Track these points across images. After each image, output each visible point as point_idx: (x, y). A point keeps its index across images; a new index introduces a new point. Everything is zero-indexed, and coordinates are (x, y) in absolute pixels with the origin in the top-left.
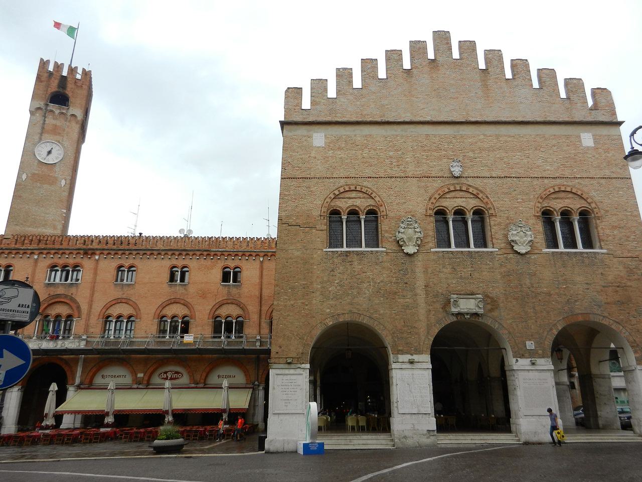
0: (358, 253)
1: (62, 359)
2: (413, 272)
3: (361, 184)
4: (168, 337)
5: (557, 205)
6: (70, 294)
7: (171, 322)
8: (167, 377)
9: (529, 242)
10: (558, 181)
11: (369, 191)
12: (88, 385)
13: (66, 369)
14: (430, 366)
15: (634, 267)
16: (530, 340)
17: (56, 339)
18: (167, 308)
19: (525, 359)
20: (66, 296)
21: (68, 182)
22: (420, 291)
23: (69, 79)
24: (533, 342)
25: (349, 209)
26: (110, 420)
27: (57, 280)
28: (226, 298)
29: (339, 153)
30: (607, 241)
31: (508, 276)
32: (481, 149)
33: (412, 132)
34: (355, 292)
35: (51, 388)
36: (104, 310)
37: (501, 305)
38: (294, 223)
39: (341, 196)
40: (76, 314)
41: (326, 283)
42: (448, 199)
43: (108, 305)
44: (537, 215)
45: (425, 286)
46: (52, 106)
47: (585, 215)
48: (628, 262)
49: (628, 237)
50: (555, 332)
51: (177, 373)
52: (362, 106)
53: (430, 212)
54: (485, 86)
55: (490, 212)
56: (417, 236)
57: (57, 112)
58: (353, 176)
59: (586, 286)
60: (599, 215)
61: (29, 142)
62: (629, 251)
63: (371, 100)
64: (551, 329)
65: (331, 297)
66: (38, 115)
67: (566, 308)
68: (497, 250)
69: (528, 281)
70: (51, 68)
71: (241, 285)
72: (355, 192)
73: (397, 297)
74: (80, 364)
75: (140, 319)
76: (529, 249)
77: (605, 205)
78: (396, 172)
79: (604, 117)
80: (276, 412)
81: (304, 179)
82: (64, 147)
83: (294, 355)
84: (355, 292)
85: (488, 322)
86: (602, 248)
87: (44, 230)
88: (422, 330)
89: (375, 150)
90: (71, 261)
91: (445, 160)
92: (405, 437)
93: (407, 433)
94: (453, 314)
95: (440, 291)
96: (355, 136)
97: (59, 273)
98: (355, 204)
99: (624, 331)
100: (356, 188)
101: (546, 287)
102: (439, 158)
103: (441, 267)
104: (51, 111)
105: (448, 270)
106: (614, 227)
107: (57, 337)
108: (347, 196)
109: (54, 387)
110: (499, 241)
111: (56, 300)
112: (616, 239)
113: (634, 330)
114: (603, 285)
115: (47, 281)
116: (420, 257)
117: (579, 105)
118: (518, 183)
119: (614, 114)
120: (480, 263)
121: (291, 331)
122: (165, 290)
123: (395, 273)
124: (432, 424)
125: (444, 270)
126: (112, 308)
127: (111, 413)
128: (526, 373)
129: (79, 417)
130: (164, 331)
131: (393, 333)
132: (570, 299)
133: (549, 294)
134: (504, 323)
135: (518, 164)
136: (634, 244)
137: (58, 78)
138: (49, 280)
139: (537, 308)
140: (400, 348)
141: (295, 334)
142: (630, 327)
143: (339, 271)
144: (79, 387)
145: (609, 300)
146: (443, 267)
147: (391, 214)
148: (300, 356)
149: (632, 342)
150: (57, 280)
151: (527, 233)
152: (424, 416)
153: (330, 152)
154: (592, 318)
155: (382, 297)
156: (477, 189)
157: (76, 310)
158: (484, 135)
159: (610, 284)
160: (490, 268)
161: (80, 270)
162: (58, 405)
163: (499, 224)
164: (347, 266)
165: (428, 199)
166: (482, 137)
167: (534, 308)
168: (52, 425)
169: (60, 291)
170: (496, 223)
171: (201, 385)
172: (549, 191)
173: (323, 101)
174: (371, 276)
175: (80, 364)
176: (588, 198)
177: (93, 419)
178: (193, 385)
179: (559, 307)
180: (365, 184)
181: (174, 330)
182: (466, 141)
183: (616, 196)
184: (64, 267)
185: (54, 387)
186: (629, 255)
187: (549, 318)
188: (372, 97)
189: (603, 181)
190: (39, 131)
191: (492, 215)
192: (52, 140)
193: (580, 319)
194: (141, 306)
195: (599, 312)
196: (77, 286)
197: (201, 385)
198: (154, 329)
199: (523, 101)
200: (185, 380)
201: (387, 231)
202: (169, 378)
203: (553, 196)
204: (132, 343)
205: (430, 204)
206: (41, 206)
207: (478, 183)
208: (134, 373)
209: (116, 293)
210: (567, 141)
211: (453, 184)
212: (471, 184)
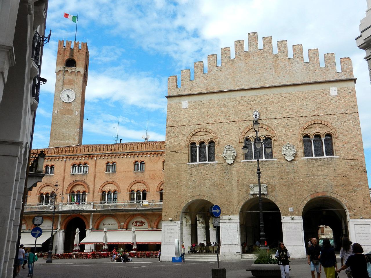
0: (204, 165)
1: (82, 215)
2: (231, 173)
3: (206, 127)
4: (135, 202)
5: (312, 132)
6: (83, 180)
7: (137, 194)
8: (137, 224)
9: (293, 154)
10: (314, 118)
11: (210, 131)
12: (97, 228)
13: (85, 220)
14: (239, 221)
15: (354, 165)
16: (291, 207)
17: (78, 205)
18: (134, 185)
19: (288, 217)
20: (81, 181)
21: (79, 112)
22: (235, 183)
23: (75, 50)
24: (293, 208)
25: (200, 141)
26: (105, 247)
27: (76, 172)
29: (195, 111)
32: (271, 103)
33: (234, 96)
34: (202, 184)
35: (76, 231)
36: (101, 188)
37: (277, 189)
38: (173, 150)
40: (87, 191)
41: (188, 180)
42: (251, 133)
43: (103, 185)
44: (300, 138)
45: (237, 180)
46: (68, 69)
47: (329, 136)
48: (352, 162)
49: (353, 148)
50: (306, 202)
51: (142, 222)
53: (241, 140)
54: (276, 63)
56: (233, 155)
57: (70, 71)
58: (202, 123)
59: (324, 177)
60: (336, 136)
61: (57, 91)
62: (352, 156)
63: (213, 79)
64: (303, 201)
65: (190, 188)
66: (61, 74)
67: (312, 189)
68: (276, 159)
70: (65, 45)
72: (203, 132)
73: (223, 186)
74: (91, 217)
75: (120, 192)
76: (293, 158)
77: (340, 130)
78: (224, 119)
79: (345, 76)
80: (165, 243)
81: (178, 127)
82: (75, 92)
83: (173, 217)
84: (202, 184)
85: (269, 197)
86: (336, 155)
87: (69, 142)
88: (235, 203)
90: (83, 161)
91: (251, 111)
92: (225, 255)
93: (226, 254)
94: (251, 194)
96: (203, 101)
97: (77, 168)
98: (203, 138)
99: (344, 201)
100: (203, 130)
101: (302, 179)
102: (247, 110)
103: (246, 170)
104: (67, 71)
105: (250, 171)
106: (345, 143)
107: (79, 203)
109: (77, 231)
110: (278, 154)
111: (77, 183)
112: (345, 149)
113: (350, 200)
114: (335, 176)
115: (71, 173)
116: (235, 165)
117: (330, 70)
118: (291, 120)
119: (352, 73)
120: (266, 167)
121: (172, 205)
122: (132, 176)
123: (222, 174)
124: (239, 249)
125: (248, 171)
126: (105, 187)
127: (106, 244)
128: (288, 224)
129: (93, 246)
130: (133, 199)
132: (315, 184)
133: (304, 182)
134: (278, 198)
137: (70, 50)
138: (73, 173)
139: (296, 190)
140: (224, 212)
141: (173, 206)
144: (92, 230)
145: (337, 184)
146: (247, 170)
147: (221, 143)
148: (176, 217)
149: (349, 207)
150: (76, 172)
151: (292, 149)
152: (235, 245)
153: (191, 111)
155: (215, 187)
156: (267, 126)
157: (87, 188)
158: (274, 94)
159: (339, 175)
161: (87, 166)
162: (81, 240)
163: (279, 145)
164: (198, 172)
165: (240, 133)
166: (272, 95)
167: (295, 190)
168: (78, 250)
169: (78, 178)
171: (155, 229)
173: (187, 82)
174: (210, 176)
175: (91, 217)
176: (331, 126)
177: (98, 246)
178: (150, 229)
179: (309, 189)
180: (208, 127)
181: (138, 198)
182: (263, 98)
183: (348, 124)
184: (79, 165)
185: (77, 231)
186: (352, 158)
187: (303, 195)
188: (213, 77)
189: (341, 116)
190: (62, 84)
191: (275, 140)
192: (69, 88)
193: (320, 195)
194: (120, 185)
195: (331, 191)
196: (87, 175)
197: (124, 230)
198: (127, 198)
199: (297, 71)
200: (146, 226)
201: (218, 152)
202: (138, 225)
203: (311, 127)
204: (116, 206)
206: (66, 128)
207: (268, 122)
208: (119, 222)
209: (106, 178)
210: (322, 93)
212: (264, 123)
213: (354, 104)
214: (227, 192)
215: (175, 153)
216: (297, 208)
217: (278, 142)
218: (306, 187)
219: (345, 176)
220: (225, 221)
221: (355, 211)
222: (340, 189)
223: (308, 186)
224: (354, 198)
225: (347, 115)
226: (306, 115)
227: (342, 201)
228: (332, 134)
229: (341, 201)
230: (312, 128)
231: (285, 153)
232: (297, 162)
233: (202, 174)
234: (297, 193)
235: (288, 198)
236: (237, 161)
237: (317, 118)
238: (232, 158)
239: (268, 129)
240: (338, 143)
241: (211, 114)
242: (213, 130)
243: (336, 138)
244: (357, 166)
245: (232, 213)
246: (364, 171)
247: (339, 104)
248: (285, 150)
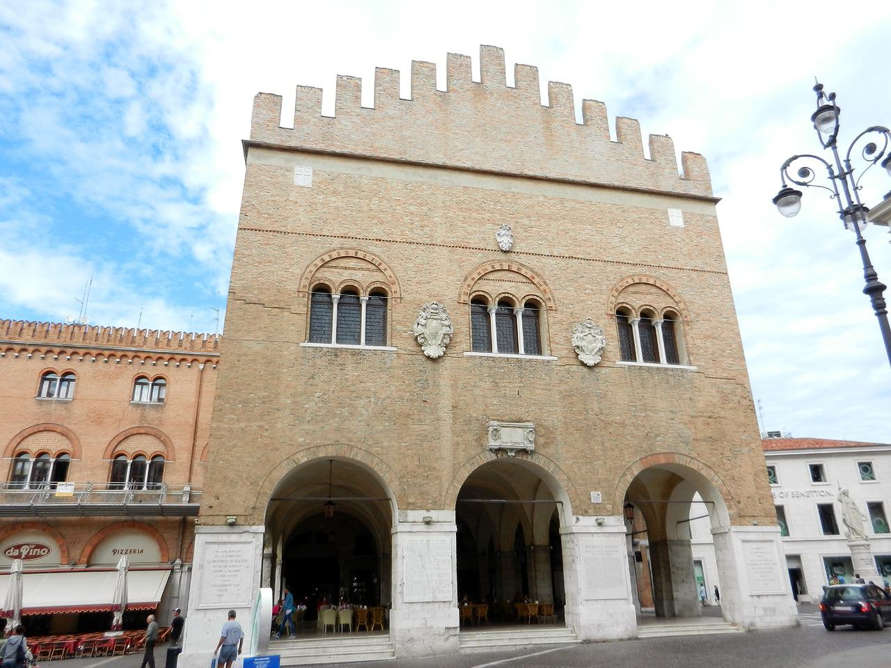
10: (638, 270)
22: (445, 414)
24: (600, 493)
28: (138, 425)
30: (697, 355)
38: (254, 300)
39: (333, 264)
44: (610, 313)
45: (453, 407)
49: (724, 351)
55: (549, 304)
59: (670, 415)
62: (724, 370)
64: (624, 475)
69: (595, 406)
71: (164, 406)
73: (410, 422)
76: (598, 359)
89: (389, 201)
95: (474, 415)
105: (487, 384)
108: (342, 265)
116: (447, 363)
118: (587, 267)
125: (481, 383)
133: (623, 425)
134: (561, 464)
140: (411, 500)
141: (245, 476)
142: (724, 473)
143: (322, 378)
146: (481, 380)
153: (320, 197)
159: (701, 414)
167: (602, 444)
172: (627, 282)
173: (314, 120)
180: (371, 249)
186: (725, 375)
189: (694, 274)
191: (550, 309)
193: (663, 460)
201: (399, 323)
215: (260, 307)
217: (559, 316)
218: (628, 437)
220: (416, 528)
221: (741, 506)
222: (705, 447)
223: (633, 436)
231: (580, 344)
232: (607, 370)
235: (587, 464)
237: (645, 270)
238: (442, 341)
240: (692, 337)
244: (736, 395)
245: (434, 503)
248: (582, 335)
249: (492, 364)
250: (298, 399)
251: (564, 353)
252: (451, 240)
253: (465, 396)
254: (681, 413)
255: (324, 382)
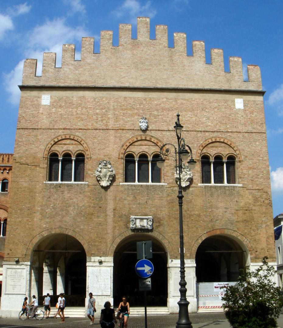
2: (106, 199)
10: (215, 134)
22: (110, 213)
30: (243, 178)
31: (172, 202)
39: (59, 143)
42: (136, 147)
45: (114, 209)
49: (258, 175)
50: (200, 241)
52: (80, 74)
53: (122, 156)
59: (225, 210)
62: (257, 185)
67: (209, 225)
68: (167, 184)
73: (93, 217)
76: (188, 183)
89: (86, 108)
103: (126, 196)
105: (131, 198)
108: (64, 143)
116: (112, 188)
118: (187, 135)
123: (93, 200)
125: (128, 198)
131: (89, 242)
133: (199, 216)
135: (189, 120)
136: (261, 180)
139: (189, 225)
140: (93, 252)
142: (250, 237)
143: (54, 198)
153: (54, 110)
154: (228, 232)
159: (242, 209)
160: (160, 197)
167: (188, 226)
170: (168, 164)
173: (51, 70)
174: (76, 202)
176: (234, 147)
180: (77, 134)
182: (153, 102)
183: (254, 145)
186: (257, 188)
188: (87, 67)
189: (246, 135)
193: (218, 233)
201: (89, 170)
205: (123, 150)
210: (225, 104)
211: (141, 135)
213: (261, 122)
214: (100, 224)
216: (190, 249)
219: (247, 210)
220: (95, 264)
221: (257, 253)
222: (241, 225)
223: (204, 221)
224: (257, 237)
225: (254, 134)
226: (206, 129)
227: (244, 241)
228: (236, 157)
229: (242, 240)
230: (212, 147)
232: (193, 189)
233: (65, 198)
234: (190, 230)
236: (115, 184)
238: (109, 179)
239: (158, 143)
240: (242, 169)
241: (83, 116)
242: (84, 138)
243: (240, 161)
244: (262, 198)
246: (270, 204)
247: (246, 120)
249: (134, 188)
250: (43, 208)
251: (171, 181)
252: (117, 126)
253: (120, 204)
254: (231, 209)
255: (54, 199)
